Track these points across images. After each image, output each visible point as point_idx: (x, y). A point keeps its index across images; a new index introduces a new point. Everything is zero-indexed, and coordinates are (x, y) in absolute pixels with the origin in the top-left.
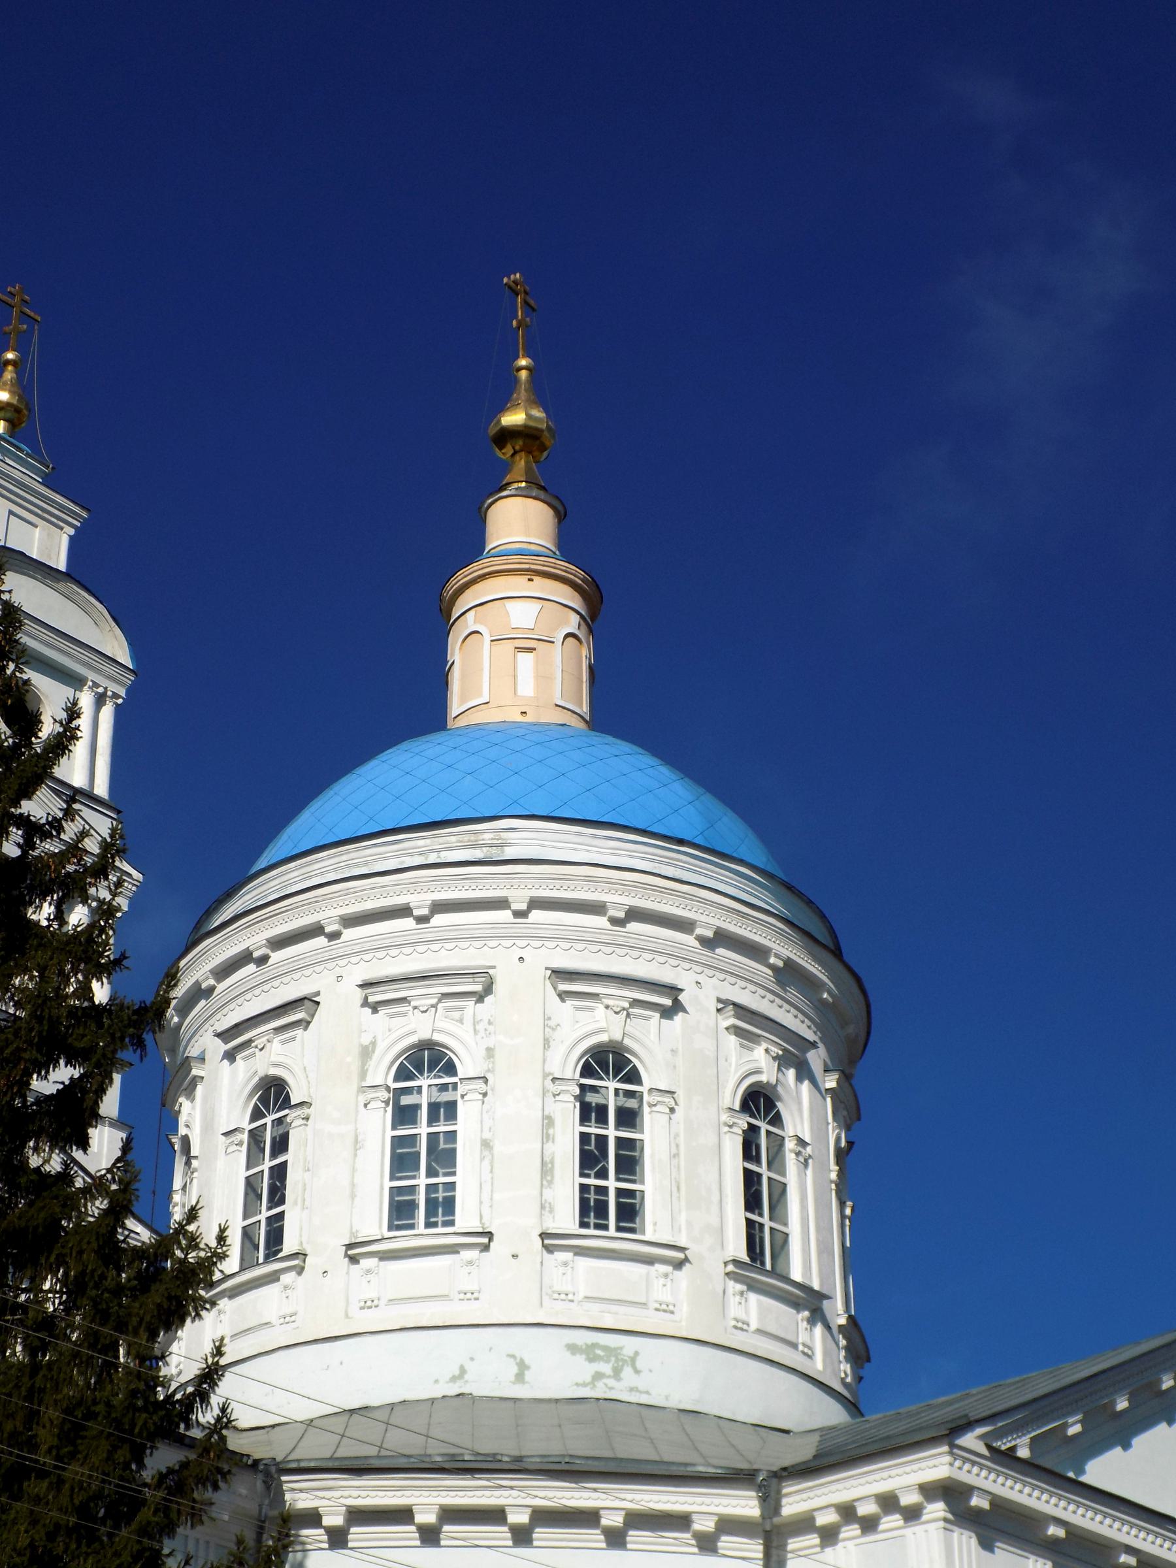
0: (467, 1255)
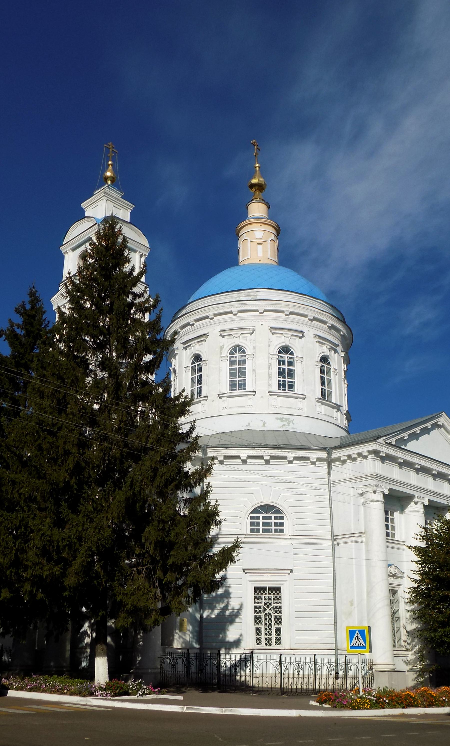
0: (249, 396)
